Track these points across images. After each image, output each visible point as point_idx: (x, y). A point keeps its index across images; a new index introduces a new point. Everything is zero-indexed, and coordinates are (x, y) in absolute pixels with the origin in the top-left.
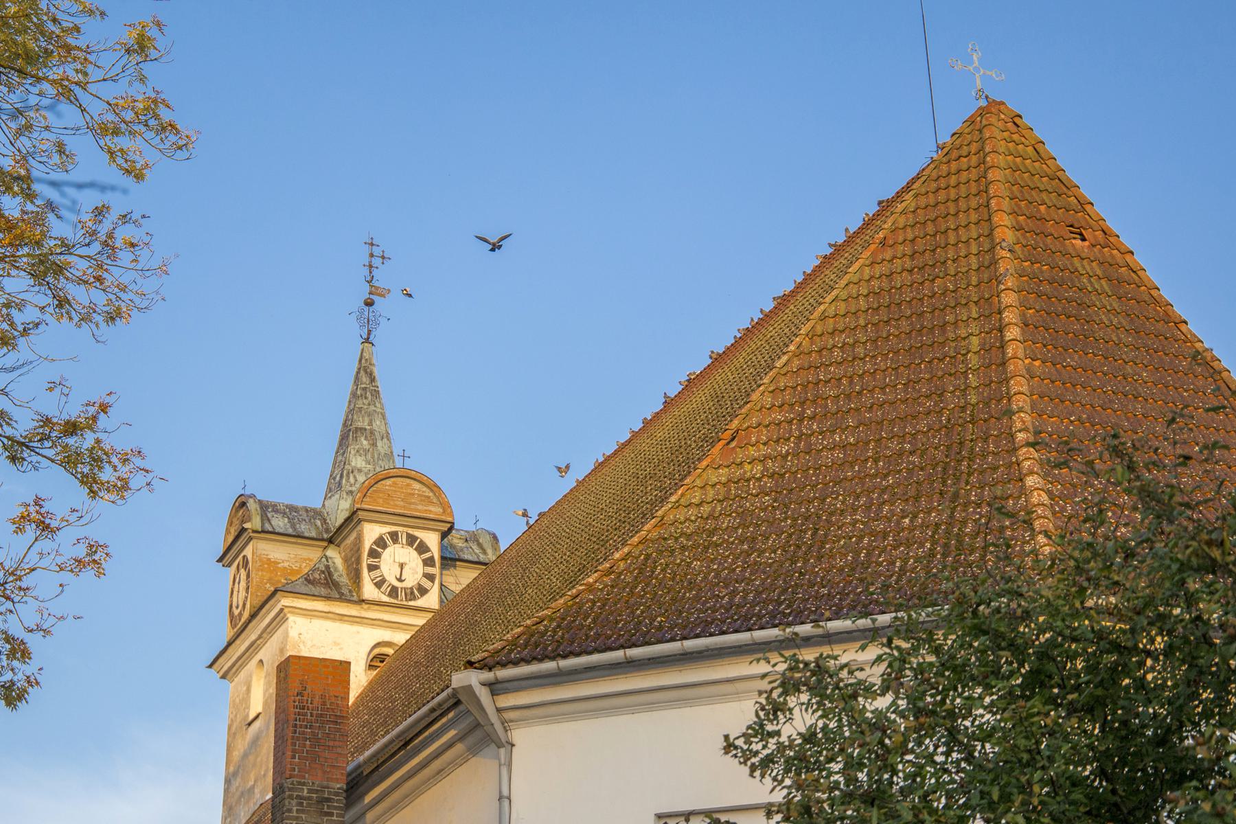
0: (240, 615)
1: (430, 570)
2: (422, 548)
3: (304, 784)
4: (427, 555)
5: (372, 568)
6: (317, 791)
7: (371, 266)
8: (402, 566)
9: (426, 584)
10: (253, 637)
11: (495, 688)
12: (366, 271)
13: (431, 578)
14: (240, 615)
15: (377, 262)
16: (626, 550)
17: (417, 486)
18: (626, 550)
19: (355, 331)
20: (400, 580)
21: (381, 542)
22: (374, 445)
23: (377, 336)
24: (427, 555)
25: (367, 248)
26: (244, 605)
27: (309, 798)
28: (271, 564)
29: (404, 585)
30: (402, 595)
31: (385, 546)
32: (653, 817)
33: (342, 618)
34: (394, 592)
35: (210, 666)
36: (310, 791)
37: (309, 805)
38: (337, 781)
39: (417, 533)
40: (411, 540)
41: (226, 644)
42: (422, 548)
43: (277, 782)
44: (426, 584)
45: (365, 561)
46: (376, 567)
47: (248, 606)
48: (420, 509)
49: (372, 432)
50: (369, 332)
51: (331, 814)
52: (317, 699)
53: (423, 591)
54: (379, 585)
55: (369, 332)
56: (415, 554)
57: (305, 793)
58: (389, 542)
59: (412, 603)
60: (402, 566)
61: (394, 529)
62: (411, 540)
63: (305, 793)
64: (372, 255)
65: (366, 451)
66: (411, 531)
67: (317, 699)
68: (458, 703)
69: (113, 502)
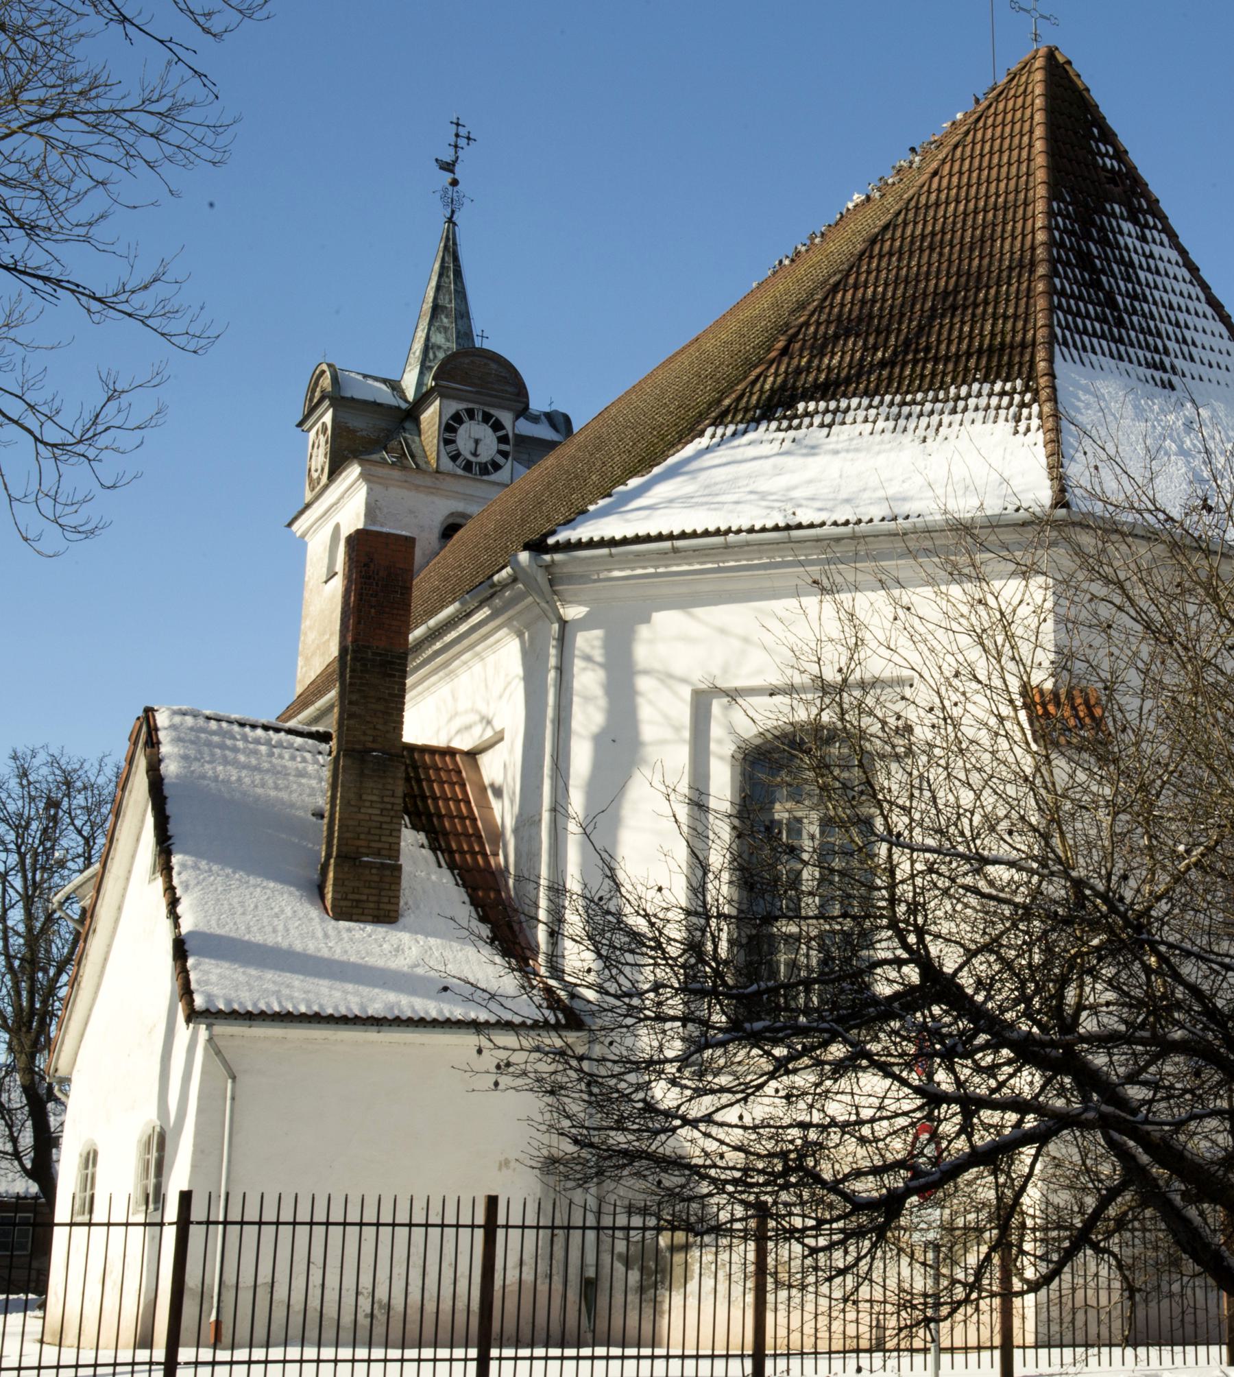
1: (504, 447)
2: (497, 426)
7: (456, 146)
13: (505, 454)
15: (462, 142)
29: (478, 460)
31: (461, 422)
36: (374, 654)
39: (492, 411)
40: (487, 418)
42: (497, 426)
46: (453, 442)
50: (453, 212)
55: (453, 212)
56: (490, 431)
58: (465, 418)
60: (477, 442)
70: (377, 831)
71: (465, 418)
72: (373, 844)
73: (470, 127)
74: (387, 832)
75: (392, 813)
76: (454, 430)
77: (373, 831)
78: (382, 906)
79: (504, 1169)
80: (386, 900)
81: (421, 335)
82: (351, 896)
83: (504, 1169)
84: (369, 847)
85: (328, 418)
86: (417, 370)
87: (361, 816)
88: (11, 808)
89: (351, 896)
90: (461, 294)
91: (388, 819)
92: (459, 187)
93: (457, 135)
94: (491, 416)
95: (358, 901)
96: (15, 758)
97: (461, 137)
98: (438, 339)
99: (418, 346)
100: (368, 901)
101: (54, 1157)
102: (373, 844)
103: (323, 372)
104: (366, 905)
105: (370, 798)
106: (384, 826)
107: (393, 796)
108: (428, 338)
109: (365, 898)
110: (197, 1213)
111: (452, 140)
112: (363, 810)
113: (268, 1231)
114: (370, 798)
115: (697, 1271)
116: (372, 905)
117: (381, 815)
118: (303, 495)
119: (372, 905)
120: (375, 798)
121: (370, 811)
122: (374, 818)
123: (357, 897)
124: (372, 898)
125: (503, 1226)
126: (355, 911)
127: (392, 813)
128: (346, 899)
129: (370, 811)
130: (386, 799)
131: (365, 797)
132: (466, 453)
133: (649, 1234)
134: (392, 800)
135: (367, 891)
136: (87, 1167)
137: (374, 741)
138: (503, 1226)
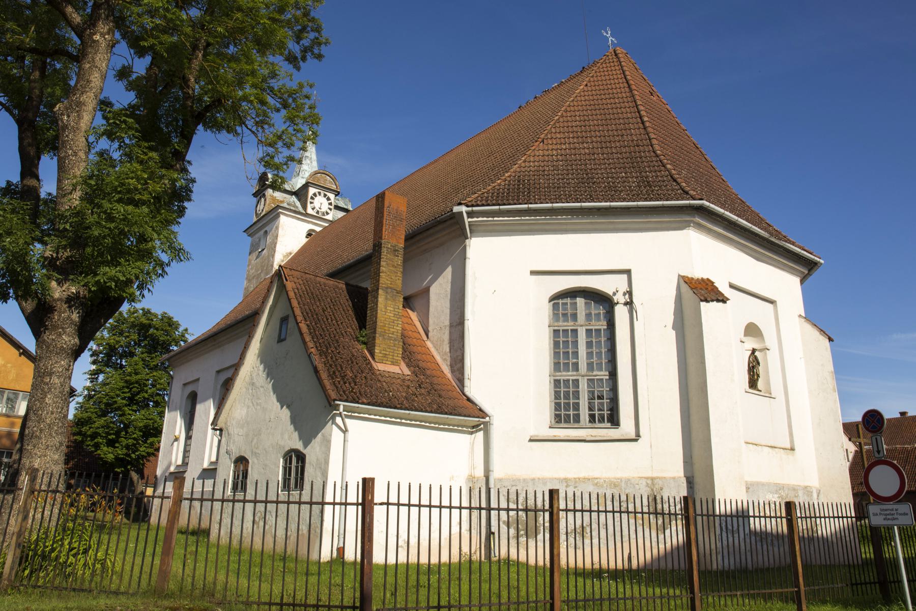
0: (261, 213)
1: (330, 207)
3: (389, 243)
4: (330, 202)
6: (393, 247)
8: (321, 204)
9: (329, 211)
10: (264, 222)
11: (470, 215)
13: (330, 209)
14: (261, 213)
16: (509, 173)
17: (328, 178)
18: (509, 173)
20: (320, 209)
21: (315, 195)
22: (311, 162)
24: (330, 202)
26: (263, 210)
27: (391, 249)
28: (274, 199)
29: (322, 210)
30: (320, 214)
31: (316, 196)
32: (215, 372)
33: (298, 219)
34: (318, 212)
35: (244, 232)
36: (391, 246)
37: (391, 251)
38: (401, 243)
40: (325, 196)
42: (328, 199)
44: (329, 211)
45: (309, 200)
47: (264, 211)
48: (328, 185)
49: (311, 158)
51: (398, 256)
52: (394, 210)
53: (327, 213)
54: (313, 209)
57: (389, 246)
58: (318, 195)
59: (323, 217)
60: (321, 204)
61: (320, 191)
62: (325, 196)
63: (389, 246)
65: (309, 164)
66: (325, 193)
67: (394, 210)
68: (454, 217)
70: (392, 324)
71: (318, 195)
74: (396, 325)
75: (398, 316)
80: (396, 355)
82: (382, 352)
87: (386, 317)
89: (382, 352)
91: (397, 319)
104: (388, 356)
105: (389, 308)
106: (395, 322)
109: (388, 353)
110: (379, 495)
112: (387, 314)
113: (414, 510)
114: (389, 308)
115: (542, 530)
116: (391, 357)
118: (253, 219)
119: (391, 357)
120: (392, 309)
121: (390, 314)
123: (385, 352)
124: (391, 354)
125: (483, 509)
126: (384, 359)
127: (398, 316)
128: (381, 353)
129: (390, 314)
130: (396, 310)
131: (388, 308)
133: (512, 513)
134: (398, 311)
135: (389, 350)
137: (391, 284)
138: (483, 509)
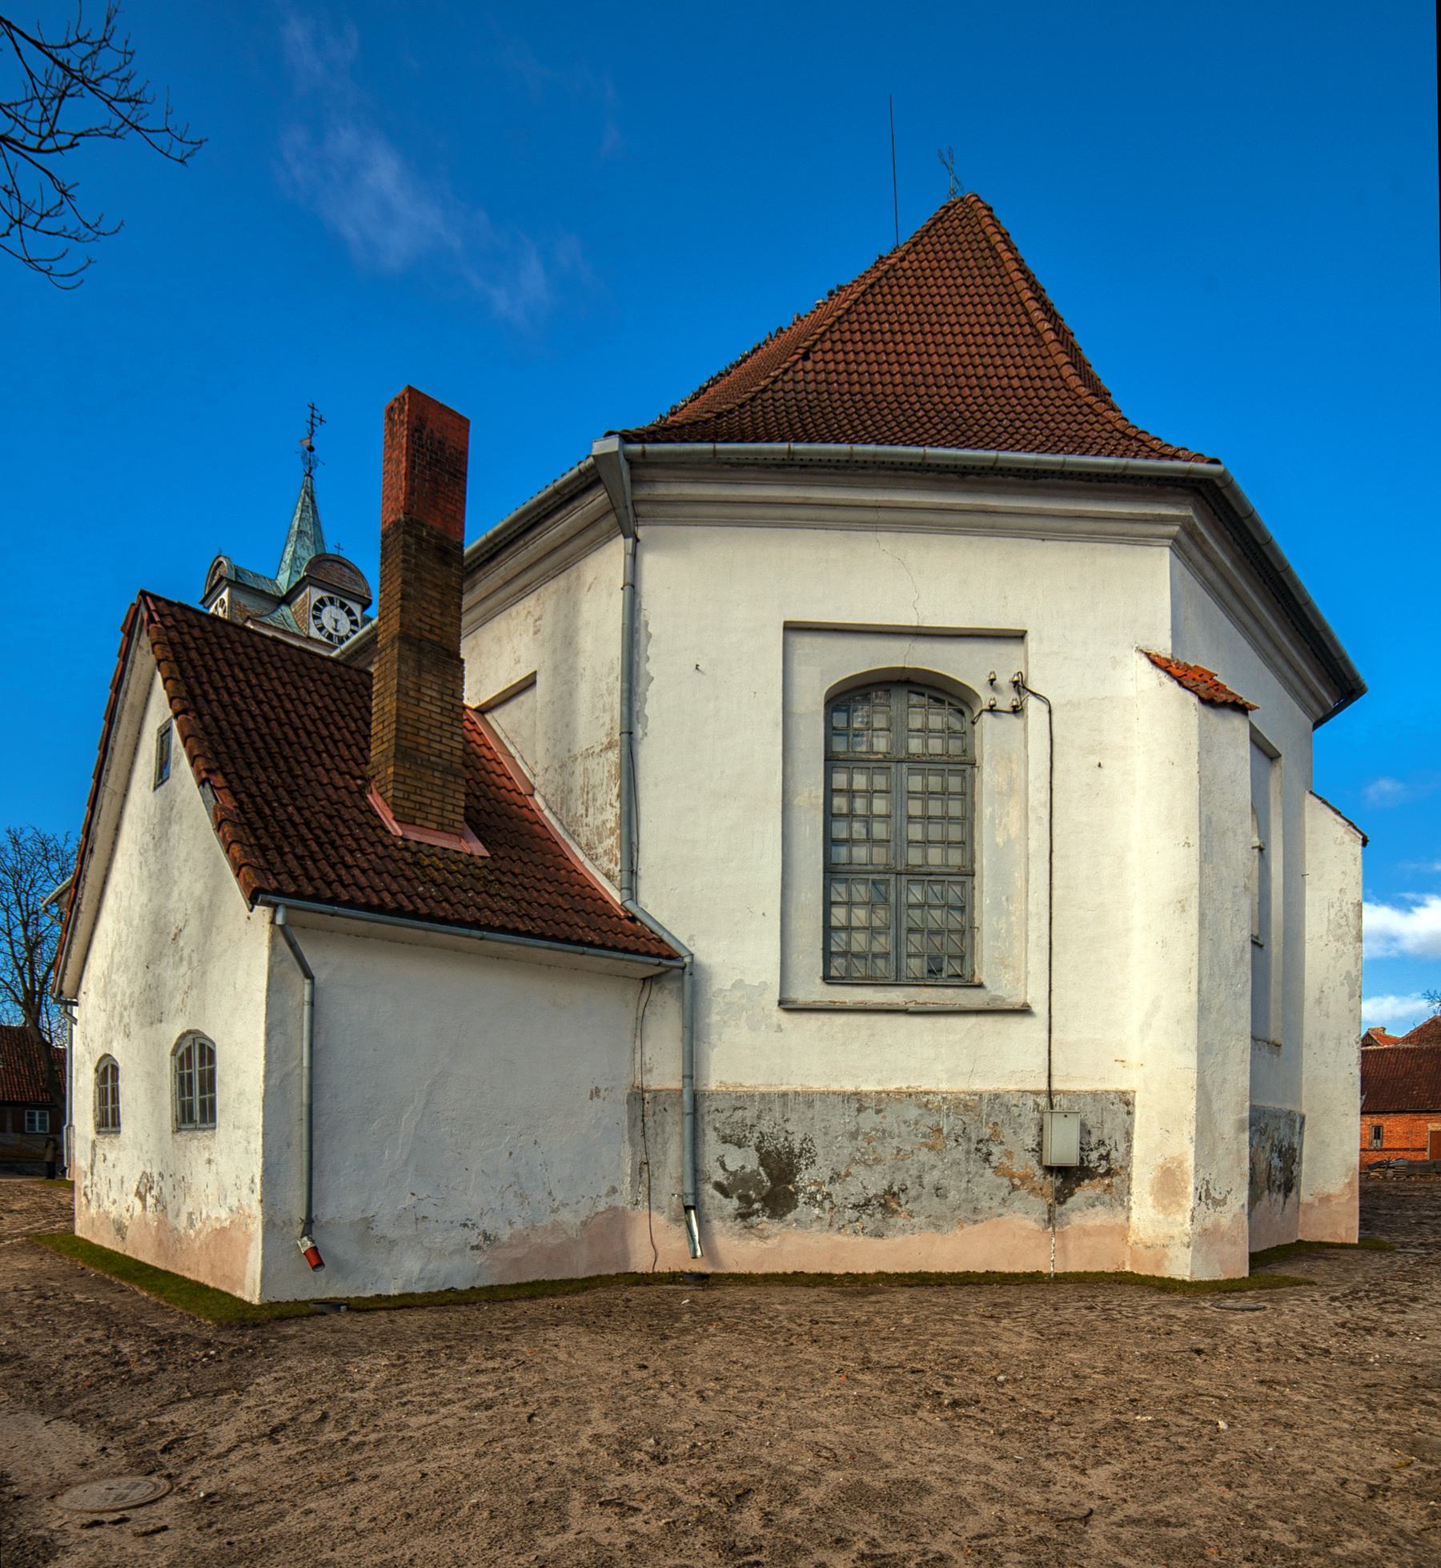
2: (350, 613)
5: (315, 617)
7: (312, 424)
12: (309, 425)
15: (316, 422)
17: (347, 571)
19: (301, 468)
20: (336, 630)
23: (315, 473)
25: (309, 410)
31: (325, 605)
34: (330, 637)
36: (428, 534)
39: (347, 602)
40: (343, 606)
41: (109, 692)
42: (350, 613)
43: (1201, 1176)
46: (319, 618)
50: (311, 469)
54: (321, 629)
55: (311, 469)
56: (345, 615)
58: (328, 603)
60: (336, 621)
64: (313, 416)
69: (181, 161)
70: (437, 731)
72: (435, 745)
73: (321, 410)
76: (320, 610)
77: (433, 730)
78: (445, 814)
79: (595, 1099)
81: (290, 549)
83: (595, 1099)
84: (429, 746)
85: (225, 596)
86: (288, 573)
88: (9, 863)
90: (317, 524)
91: (448, 721)
92: (315, 453)
93: (313, 416)
94: (345, 605)
95: (421, 804)
96: (9, 832)
97: (315, 421)
98: (302, 553)
99: (288, 557)
100: (431, 805)
101: (1414, 995)
102: (435, 745)
103: (221, 563)
104: (429, 810)
105: (429, 692)
107: (453, 696)
108: (295, 552)
111: (309, 419)
117: (441, 714)
119: (435, 811)
121: (430, 707)
122: (434, 716)
123: (419, 799)
128: (408, 799)
132: (329, 628)
136: (183, 1095)
